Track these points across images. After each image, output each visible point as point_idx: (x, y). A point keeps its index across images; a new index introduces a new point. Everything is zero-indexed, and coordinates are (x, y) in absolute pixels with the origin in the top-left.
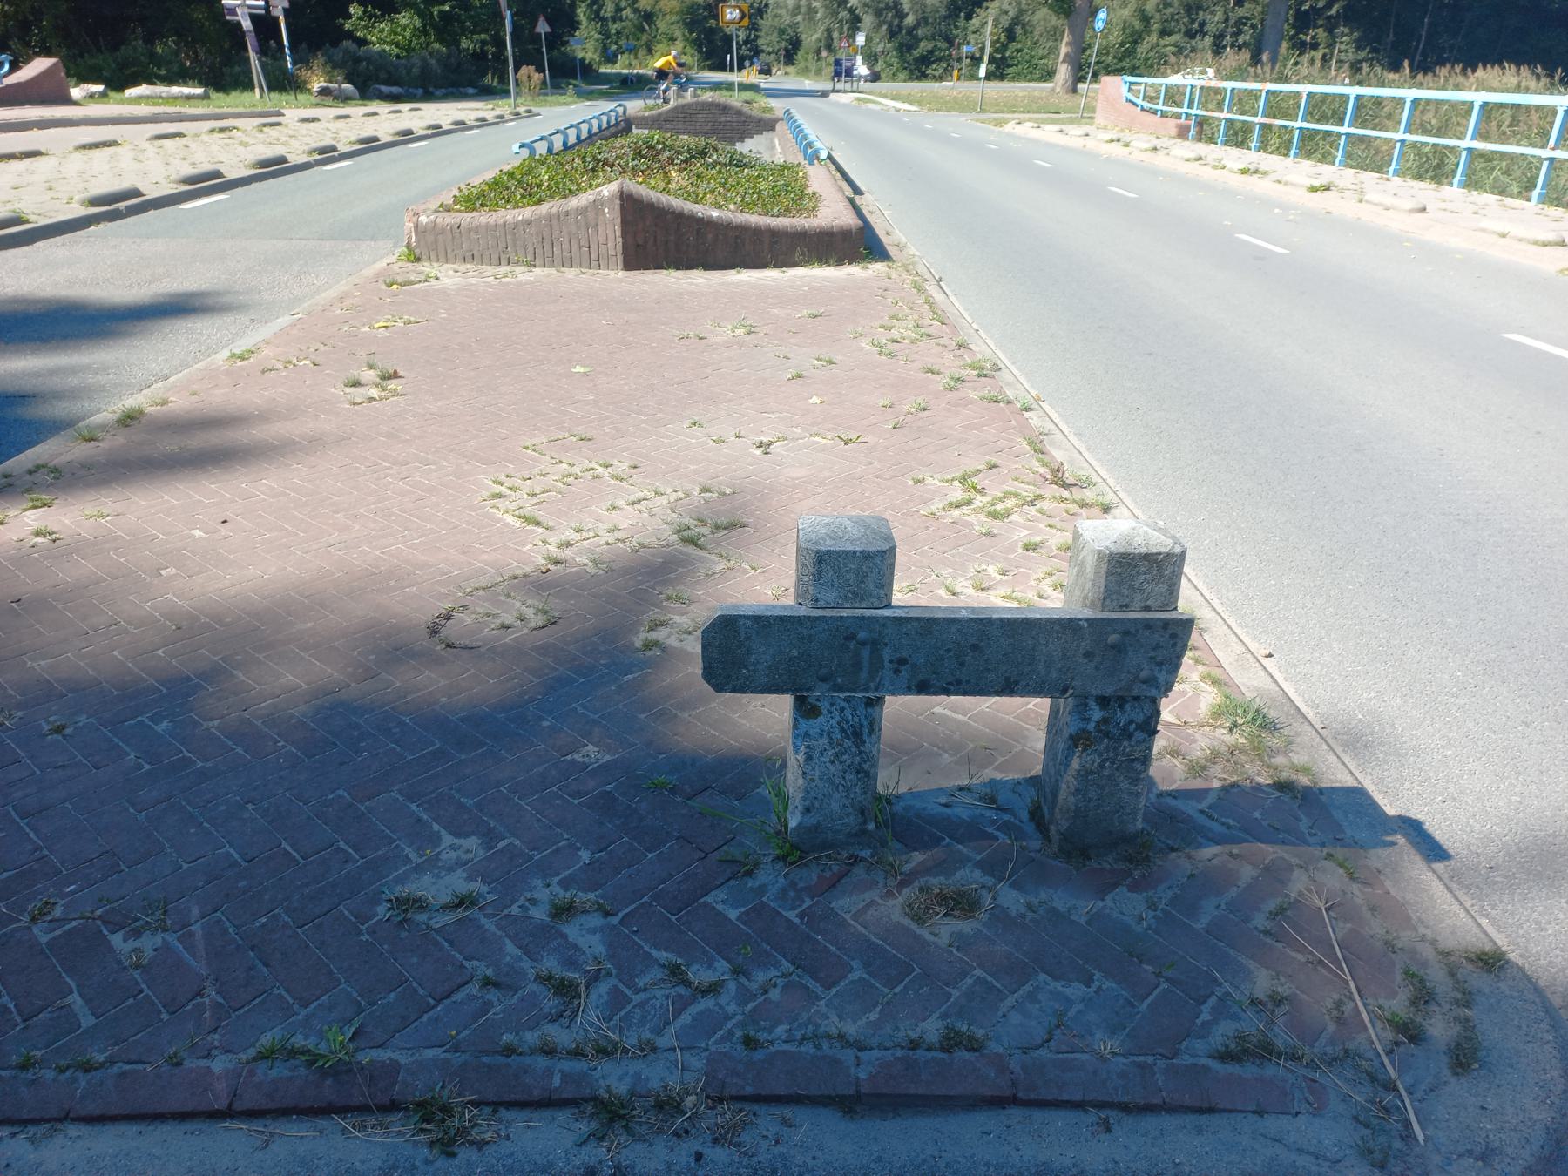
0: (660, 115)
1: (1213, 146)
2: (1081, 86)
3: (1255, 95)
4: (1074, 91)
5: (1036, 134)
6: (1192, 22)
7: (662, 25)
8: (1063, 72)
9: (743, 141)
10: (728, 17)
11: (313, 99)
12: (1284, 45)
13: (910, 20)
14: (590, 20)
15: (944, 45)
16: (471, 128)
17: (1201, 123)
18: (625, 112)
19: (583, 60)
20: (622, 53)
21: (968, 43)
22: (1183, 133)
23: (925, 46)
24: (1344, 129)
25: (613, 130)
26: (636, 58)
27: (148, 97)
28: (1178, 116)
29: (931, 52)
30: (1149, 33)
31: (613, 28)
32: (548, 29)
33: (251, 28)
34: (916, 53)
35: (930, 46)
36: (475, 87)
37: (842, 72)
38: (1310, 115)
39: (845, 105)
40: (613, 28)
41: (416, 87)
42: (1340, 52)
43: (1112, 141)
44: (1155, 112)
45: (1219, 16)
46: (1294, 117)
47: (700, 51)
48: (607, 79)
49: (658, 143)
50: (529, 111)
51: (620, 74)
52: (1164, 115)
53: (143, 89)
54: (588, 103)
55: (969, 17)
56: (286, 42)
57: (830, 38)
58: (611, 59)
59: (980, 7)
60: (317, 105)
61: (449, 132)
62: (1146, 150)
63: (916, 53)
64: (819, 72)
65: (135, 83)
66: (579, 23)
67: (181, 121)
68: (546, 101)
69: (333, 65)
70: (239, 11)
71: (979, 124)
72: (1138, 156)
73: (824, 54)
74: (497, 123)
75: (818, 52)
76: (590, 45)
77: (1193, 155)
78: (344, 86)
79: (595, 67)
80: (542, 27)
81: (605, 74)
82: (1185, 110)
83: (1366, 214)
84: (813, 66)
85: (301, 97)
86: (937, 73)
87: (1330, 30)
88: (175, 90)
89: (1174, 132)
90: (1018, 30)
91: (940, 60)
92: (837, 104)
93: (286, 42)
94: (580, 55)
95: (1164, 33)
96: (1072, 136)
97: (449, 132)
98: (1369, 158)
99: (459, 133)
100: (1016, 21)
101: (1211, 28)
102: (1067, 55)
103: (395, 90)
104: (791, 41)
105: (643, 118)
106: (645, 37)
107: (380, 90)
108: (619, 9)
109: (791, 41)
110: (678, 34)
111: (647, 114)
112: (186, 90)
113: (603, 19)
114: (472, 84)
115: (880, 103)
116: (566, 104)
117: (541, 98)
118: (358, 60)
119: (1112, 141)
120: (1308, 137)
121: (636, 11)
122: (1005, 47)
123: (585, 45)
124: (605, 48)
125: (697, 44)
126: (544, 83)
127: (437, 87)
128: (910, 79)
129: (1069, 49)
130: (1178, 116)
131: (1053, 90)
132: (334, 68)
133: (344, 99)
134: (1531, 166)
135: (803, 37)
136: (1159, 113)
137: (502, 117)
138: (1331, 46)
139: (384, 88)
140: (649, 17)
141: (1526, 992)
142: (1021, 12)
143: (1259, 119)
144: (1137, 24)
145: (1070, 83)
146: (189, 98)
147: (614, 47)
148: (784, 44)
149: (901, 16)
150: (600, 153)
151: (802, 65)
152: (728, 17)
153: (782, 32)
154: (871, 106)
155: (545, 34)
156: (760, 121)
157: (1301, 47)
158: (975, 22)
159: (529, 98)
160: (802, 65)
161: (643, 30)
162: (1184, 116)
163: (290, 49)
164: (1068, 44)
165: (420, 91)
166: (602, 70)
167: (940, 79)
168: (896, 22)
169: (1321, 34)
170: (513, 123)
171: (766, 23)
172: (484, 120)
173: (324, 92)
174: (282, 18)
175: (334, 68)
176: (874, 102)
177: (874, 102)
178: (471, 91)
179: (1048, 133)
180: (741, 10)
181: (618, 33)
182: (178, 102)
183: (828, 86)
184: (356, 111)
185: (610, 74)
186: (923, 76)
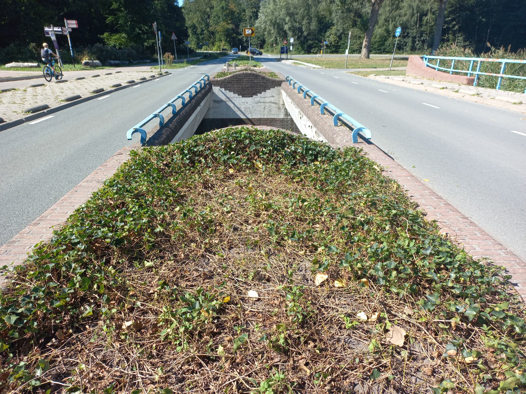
0: (225, 79)
1: (494, 90)
2: (371, 55)
4: (368, 57)
5: (387, 81)
7: (217, 36)
8: (364, 51)
9: (265, 91)
10: (247, 33)
11: (83, 67)
13: (305, 33)
14: (193, 34)
15: (317, 42)
16: (137, 84)
18: (208, 79)
19: (191, 48)
20: (204, 45)
21: (326, 41)
22: (470, 82)
24: (499, 75)
25: (203, 91)
26: (209, 47)
27: (15, 67)
28: (466, 74)
29: (312, 44)
30: (390, 37)
31: (201, 37)
32: (176, 38)
33: (55, 40)
35: (312, 42)
36: (149, 59)
37: (284, 51)
39: (289, 66)
40: (201, 37)
41: (126, 61)
42: (457, 42)
43: (443, 88)
44: (449, 73)
46: (450, 68)
47: (230, 44)
48: (199, 54)
49: (245, 138)
50: (167, 72)
51: (204, 53)
52: (439, 70)
53: (13, 64)
54: (192, 66)
55: (326, 32)
56: (70, 45)
57: (277, 40)
58: (201, 48)
59: (329, 28)
60: (83, 69)
61: (125, 87)
62: (474, 95)
64: (272, 51)
65: (10, 61)
66: (189, 35)
67: (8, 81)
68: (175, 66)
69: (92, 54)
70: (50, 33)
71: (353, 75)
73: (274, 45)
74: (151, 80)
75: (272, 45)
76: (193, 43)
77: (517, 101)
78: (94, 61)
79: (195, 50)
80: (174, 37)
81: (198, 53)
82: (470, 72)
84: (270, 49)
85: (77, 66)
86: (315, 52)
87: (454, 35)
88: (26, 64)
89: (465, 82)
91: (315, 47)
92: (286, 65)
93: (70, 45)
94: (189, 46)
96: (395, 80)
97: (125, 87)
99: (130, 87)
102: (366, 45)
103: (117, 62)
104: (261, 41)
105: (217, 81)
106: (212, 40)
107: (111, 63)
108: (203, 31)
109: (261, 41)
110: (222, 38)
111: (219, 79)
112: (30, 64)
113: (197, 34)
114: (148, 58)
115: (304, 65)
116: (183, 67)
117: (173, 64)
118: (102, 51)
119: (443, 88)
121: (208, 31)
122: (338, 42)
123: (191, 43)
124: (198, 44)
125: (230, 42)
126: (174, 59)
127: (135, 60)
128: (305, 53)
129: (367, 43)
130: (466, 74)
131: (361, 57)
132: (92, 54)
133: (94, 66)
134: (450, 71)
135: (266, 39)
136: (469, 75)
137: (153, 76)
139: (112, 62)
140: (213, 33)
144: (386, 34)
145: (367, 55)
146: (31, 67)
147: (201, 44)
148: (259, 42)
149: (302, 32)
150: (196, 146)
151: (266, 49)
152: (247, 33)
153: (258, 38)
154: (301, 66)
155: (89, 60)
156: (274, 81)
158: (328, 34)
159: (168, 65)
160: (266, 49)
161: (211, 37)
162: (469, 75)
163: (72, 47)
164: (366, 41)
165: (127, 62)
166: (197, 51)
167: (316, 53)
168: (300, 34)
169: (451, 36)
170: (158, 79)
172: (144, 79)
173: (86, 64)
174: (68, 36)
175: (92, 54)
176: (302, 64)
177: (302, 64)
178: (148, 61)
179: (381, 78)
180: (252, 30)
181: (202, 39)
182: (33, 69)
183: (278, 56)
184: (102, 72)
185: (200, 53)
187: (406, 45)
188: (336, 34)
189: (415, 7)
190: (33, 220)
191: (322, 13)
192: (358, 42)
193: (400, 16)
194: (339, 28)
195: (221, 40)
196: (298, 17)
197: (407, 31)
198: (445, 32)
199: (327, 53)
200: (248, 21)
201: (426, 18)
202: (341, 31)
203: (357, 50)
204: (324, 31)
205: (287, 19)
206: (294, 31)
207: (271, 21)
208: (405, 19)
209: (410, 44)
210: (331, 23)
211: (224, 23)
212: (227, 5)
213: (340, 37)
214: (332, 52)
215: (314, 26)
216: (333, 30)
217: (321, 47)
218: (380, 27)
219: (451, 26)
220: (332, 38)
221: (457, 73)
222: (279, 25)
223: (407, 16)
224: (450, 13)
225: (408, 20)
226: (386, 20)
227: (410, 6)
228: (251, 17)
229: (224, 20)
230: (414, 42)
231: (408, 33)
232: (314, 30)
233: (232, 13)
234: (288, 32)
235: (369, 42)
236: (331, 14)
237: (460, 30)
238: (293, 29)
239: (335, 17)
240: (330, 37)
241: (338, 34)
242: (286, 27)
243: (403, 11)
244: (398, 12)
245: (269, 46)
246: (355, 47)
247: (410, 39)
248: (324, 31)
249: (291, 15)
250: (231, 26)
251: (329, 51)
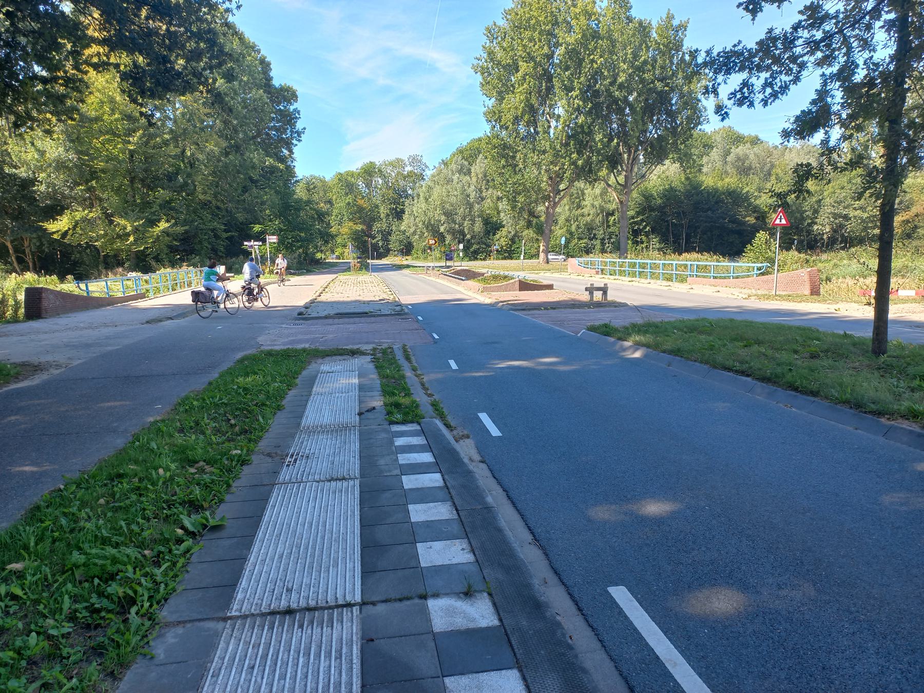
3: (635, 263)
6: (590, 234)
12: (630, 242)
13: (468, 236)
15: (484, 246)
17: (602, 270)
23: (475, 247)
34: (472, 250)
38: (629, 267)
44: (729, 277)
45: (602, 232)
55: (494, 234)
63: (472, 250)
64: (426, 258)
72: (587, 278)
83: (640, 284)
84: (422, 256)
87: (647, 236)
90: (516, 239)
91: (482, 252)
95: (580, 239)
98: (654, 276)
100: (515, 235)
101: (600, 236)
102: (543, 250)
120: (640, 273)
122: (511, 246)
128: (470, 260)
138: (648, 242)
141: (73, 651)
142: (517, 232)
143: (618, 268)
149: (464, 235)
157: (636, 243)
158: (497, 236)
160: (415, 256)
167: (484, 259)
169: (644, 238)
171: (393, 238)
186: (476, 259)
187: (594, 248)
188: (507, 237)
189: (598, 206)
190: (65, 507)
191: (488, 212)
192: (536, 245)
193: (583, 216)
194: (510, 230)
195: (344, 246)
196: (458, 219)
197: (594, 232)
198: (636, 233)
199: (498, 259)
200: (384, 220)
201: (613, 218)
202: (513, 233)
203: (535, 255)
204: (491, 234)
205: (443, 218)
206: (453, 234)
207: (424, 223)
208: (589, 219)
209: (598, 247)
210: (500, 224)
211: (351, 224)
212: (355, 200)
213: (513, 240)
214: (505, 258)
215: (478, 226)
216: (504, 232)
217: (491, 251)
218: (561, 228)
219: (641, 227)
220: (503, 242)
221: (737, 277)
222: (432, 226)
223: (591, 216)
224: (638, 213)
225: (592, 221)
226: (567, 220)
227: (593, 206)
228: (388, 215)
229: (350, 220)
230: (603, 244)
231: (595, 235)
232: (480, 232)
233: (361, 209)
234: (445, 234)
235: (547, 246)
236: (499, 213)
237: (653, 231)
238: (452, 232)
239: (505, 218)
240: (501, 239)
241: (510, 236)
242: (442, 229)
243: (585, 211)
244: (579, 211)
245: (419, 252)
246: (533, 251)
247: (598, 242)
248: (491, 234)
249: (448, 214)
250: (360, 227)
251: (500, 257)
